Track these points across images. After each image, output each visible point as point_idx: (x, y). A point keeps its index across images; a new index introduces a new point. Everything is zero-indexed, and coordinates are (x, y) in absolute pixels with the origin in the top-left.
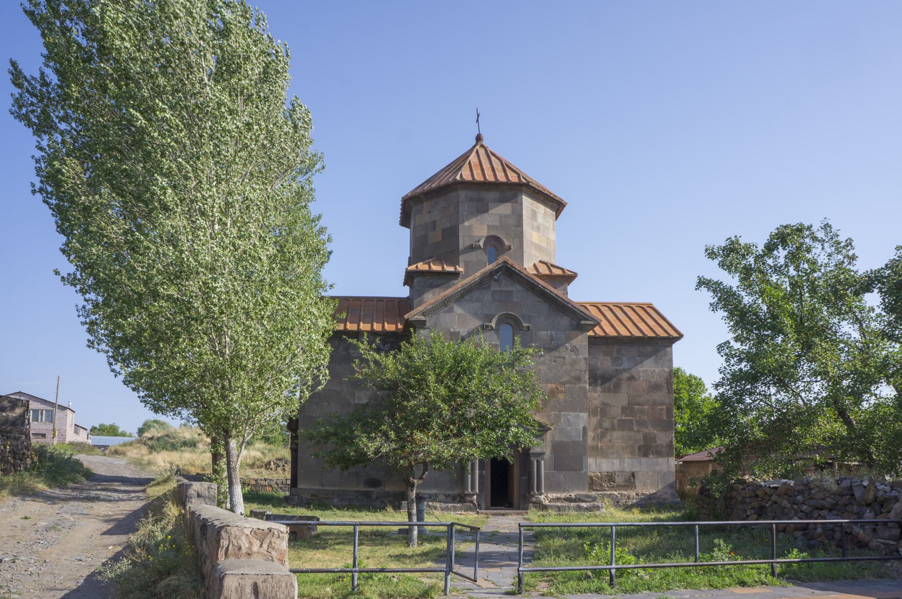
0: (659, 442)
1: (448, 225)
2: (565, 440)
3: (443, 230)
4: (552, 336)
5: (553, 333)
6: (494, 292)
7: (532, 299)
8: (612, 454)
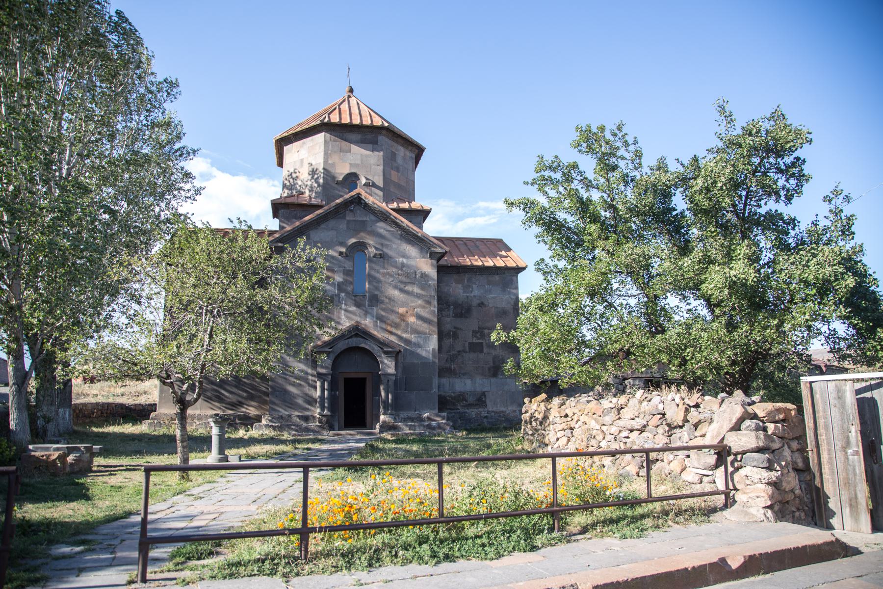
2: (416, 361)
6: (349, 222)
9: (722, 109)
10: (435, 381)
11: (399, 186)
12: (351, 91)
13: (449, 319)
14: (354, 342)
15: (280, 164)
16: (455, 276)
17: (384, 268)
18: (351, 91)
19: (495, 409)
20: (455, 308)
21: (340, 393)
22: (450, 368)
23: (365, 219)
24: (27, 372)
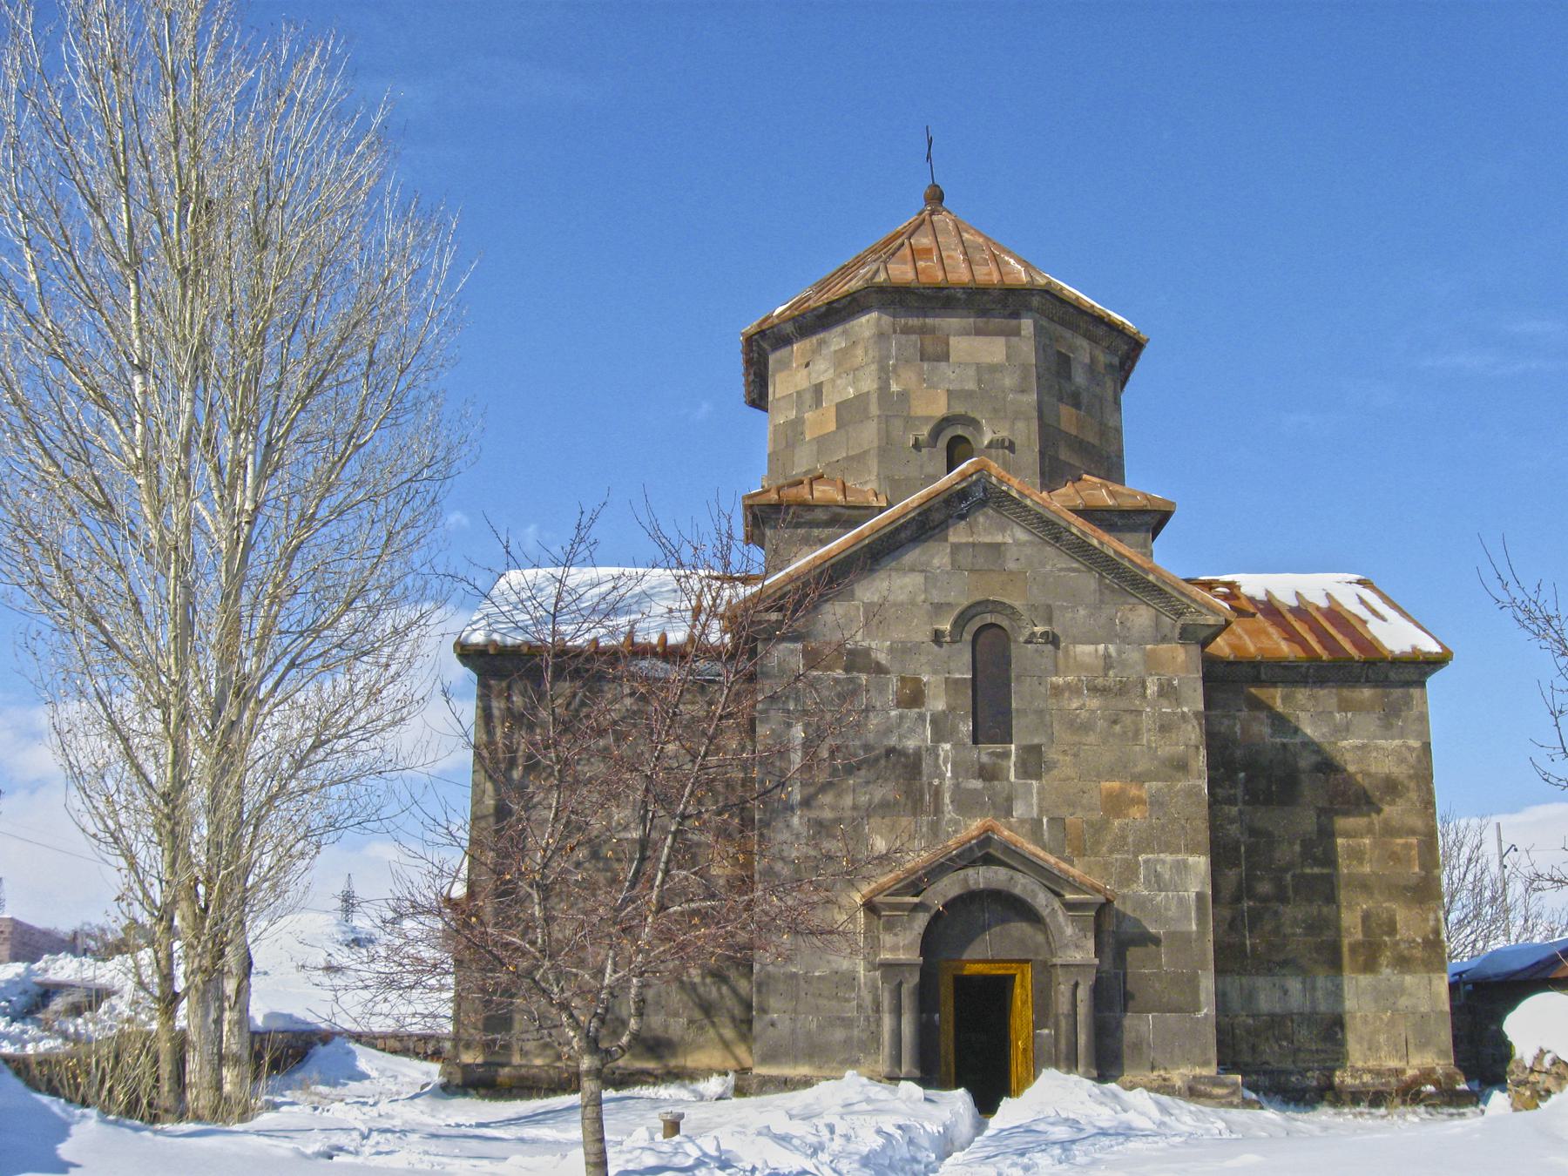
0: (1403, 933)
3: (841, 407)
4: (1107, 656)
5: (1112, 649)
6: (956, 548)
9: (266, 973)
11: (1081, 447)
12: (936, 197)
13: (1234, 810)
14: (981, 877)
15: (759, 400)
18: (936, 197)
19: (1372, 1064)
20: (1249, 779)
21: (945, 1017)
23: (999, 539)
24: (176, 995)
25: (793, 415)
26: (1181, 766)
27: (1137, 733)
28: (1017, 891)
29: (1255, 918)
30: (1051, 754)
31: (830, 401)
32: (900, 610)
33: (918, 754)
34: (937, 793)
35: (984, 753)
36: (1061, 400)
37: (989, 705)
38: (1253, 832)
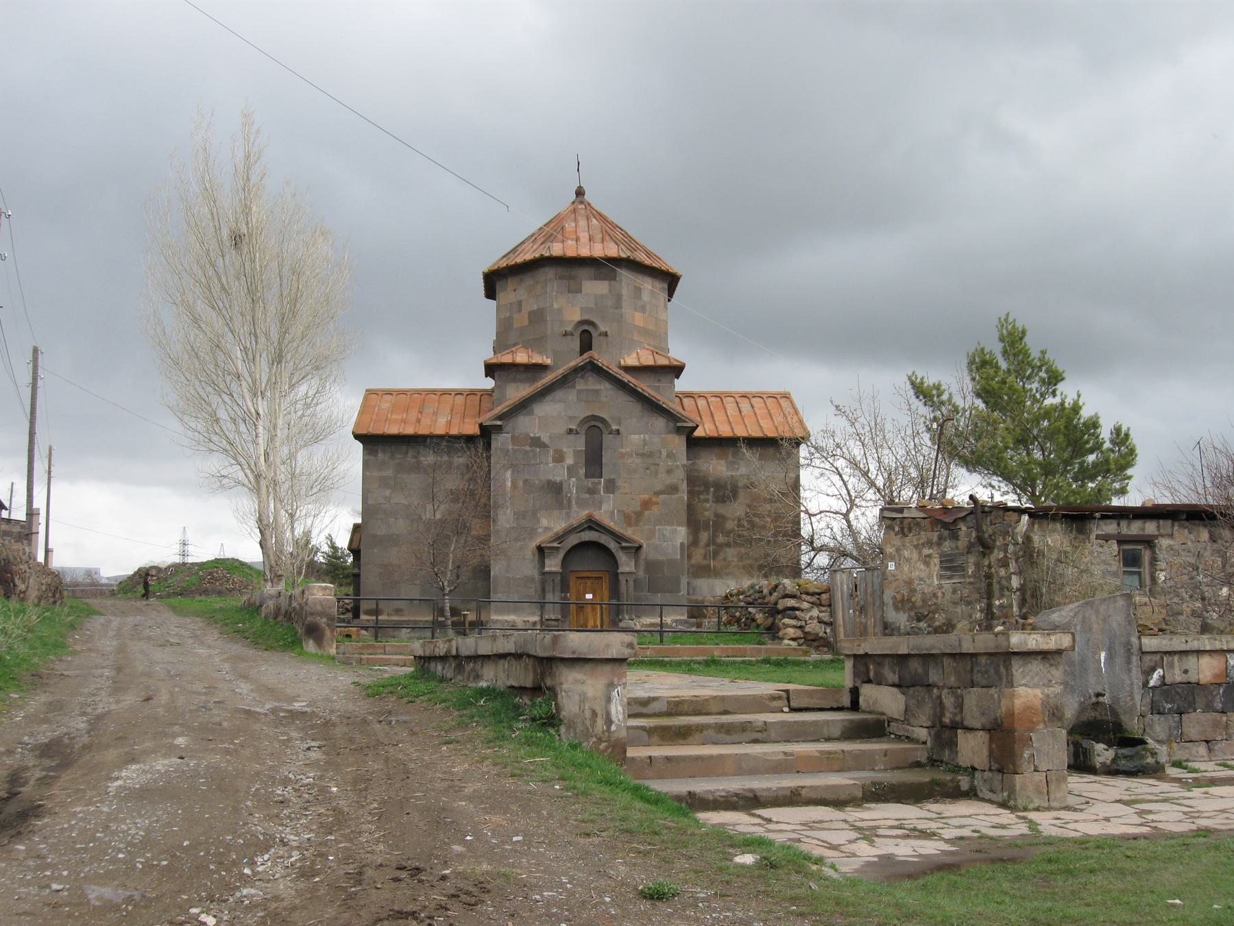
1: (535, 307)
2: (661, 558)
3: (531, 313)
4: (644, 440)
6: (579, 392)
7: (622, 399)
8: (728, 574)
10: (684, 581)
16: (716, 450)
17: (26, 782)
20: (715, 491)
22: (709, 566)
23: (598, 387)
25: (508, 315)
26: (673, 489)
27: (656, 474)
28: (602, 541)
29: (716, 554)
30: (619, 483)
31: (526, 309)
32: (554, 418)
33: (561, 483)
34: (569, 500)
35: (590, 483)
36: (635, 310)
37: (593, 460)
38: (716, 515)
